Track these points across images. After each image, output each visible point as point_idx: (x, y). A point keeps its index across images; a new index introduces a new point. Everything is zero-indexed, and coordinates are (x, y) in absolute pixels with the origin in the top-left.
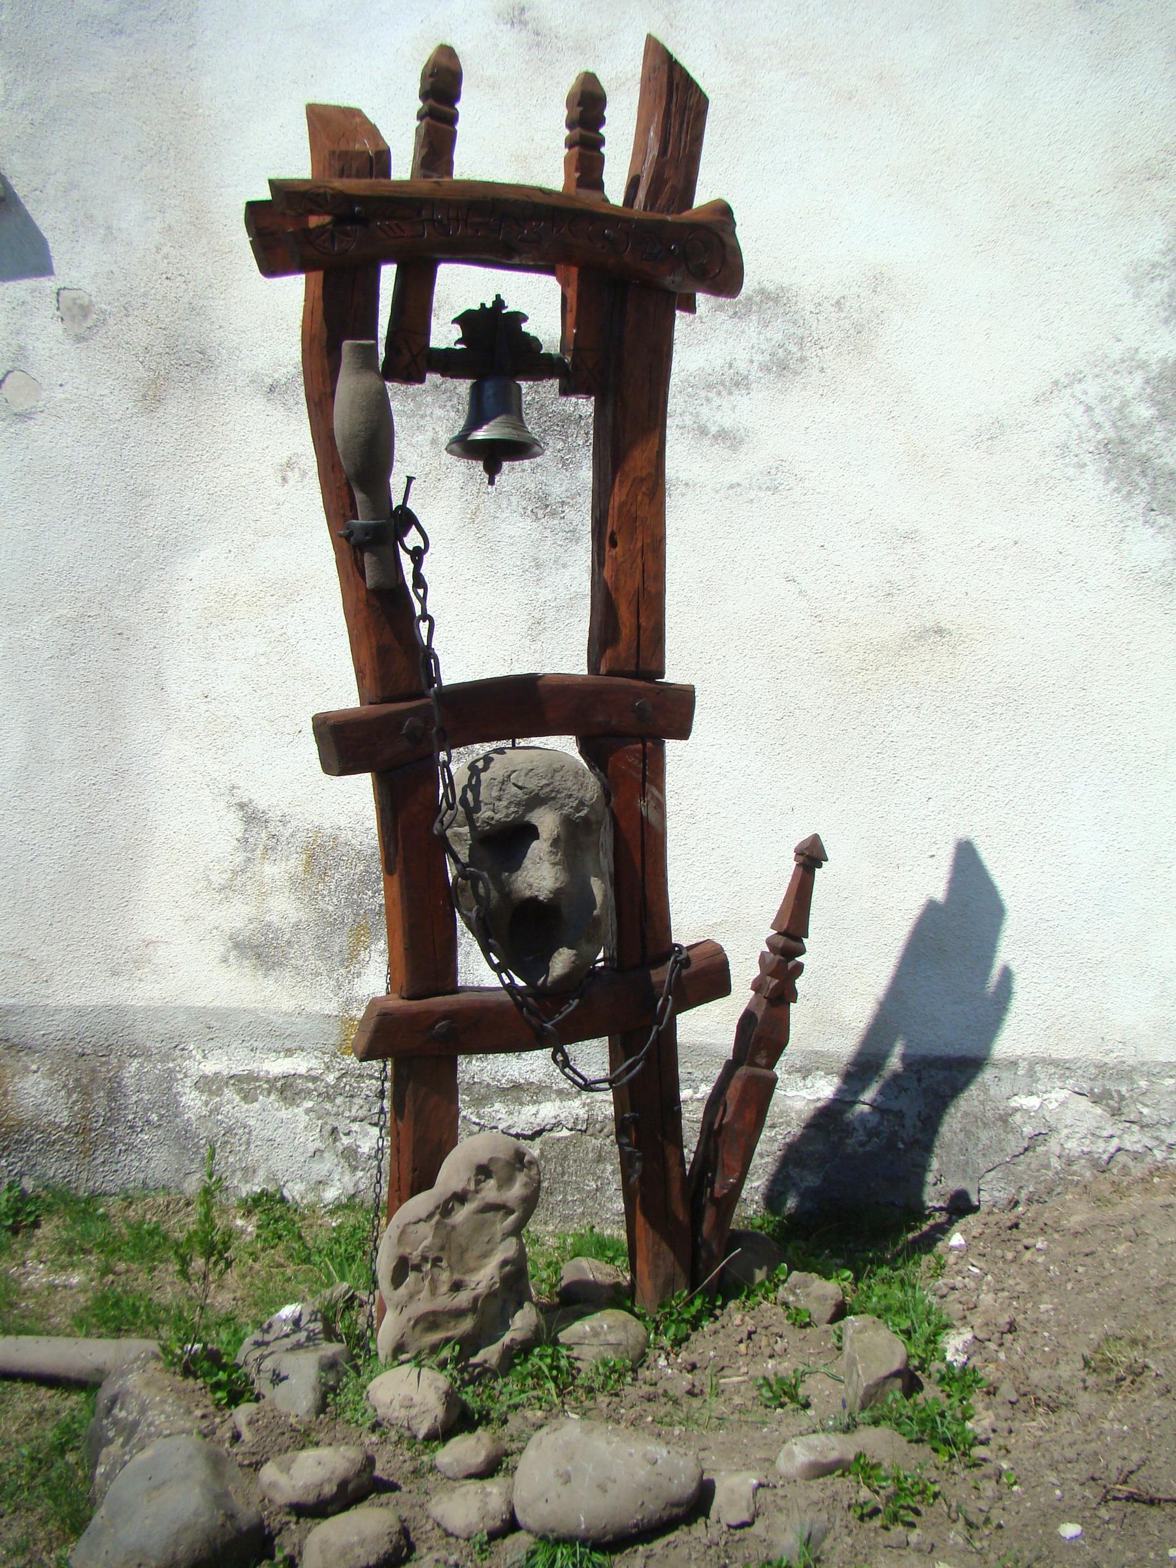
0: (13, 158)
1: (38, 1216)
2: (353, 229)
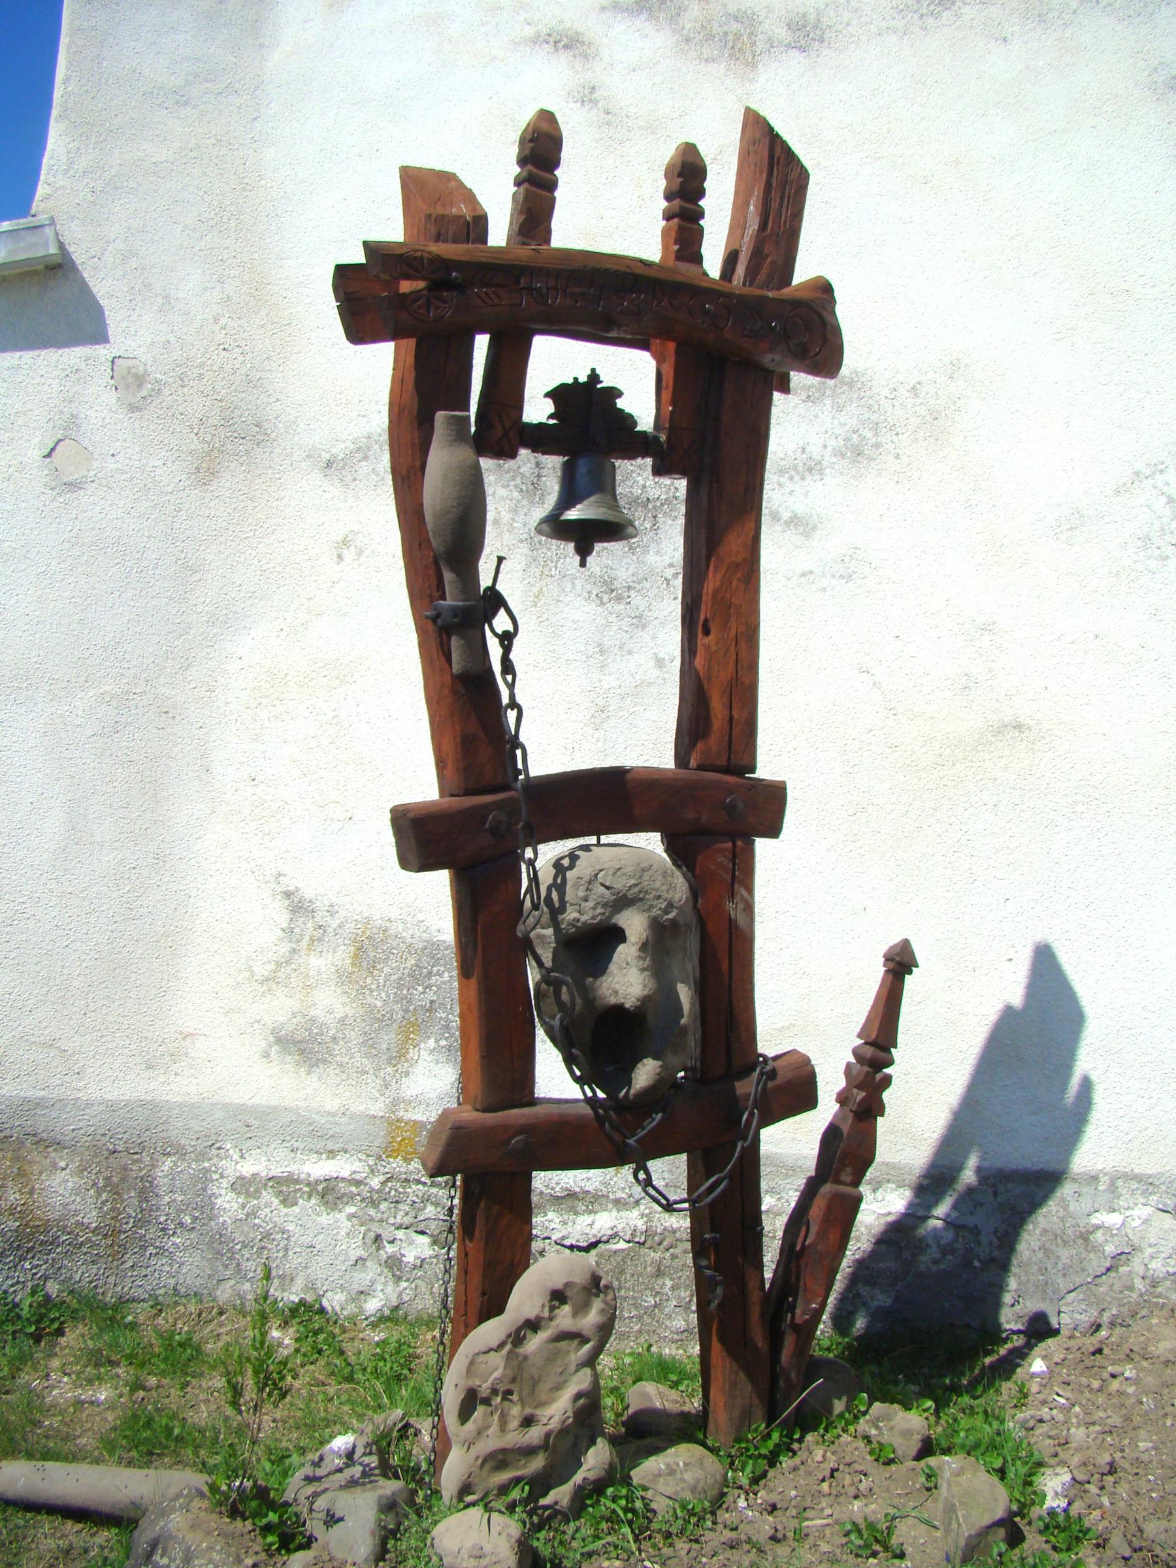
0: (73, 225)
1: (62, 1323)
2: (446, 299)
